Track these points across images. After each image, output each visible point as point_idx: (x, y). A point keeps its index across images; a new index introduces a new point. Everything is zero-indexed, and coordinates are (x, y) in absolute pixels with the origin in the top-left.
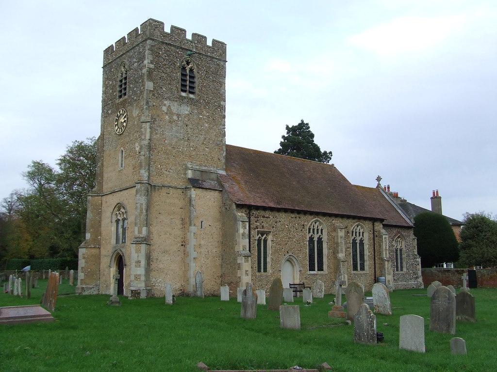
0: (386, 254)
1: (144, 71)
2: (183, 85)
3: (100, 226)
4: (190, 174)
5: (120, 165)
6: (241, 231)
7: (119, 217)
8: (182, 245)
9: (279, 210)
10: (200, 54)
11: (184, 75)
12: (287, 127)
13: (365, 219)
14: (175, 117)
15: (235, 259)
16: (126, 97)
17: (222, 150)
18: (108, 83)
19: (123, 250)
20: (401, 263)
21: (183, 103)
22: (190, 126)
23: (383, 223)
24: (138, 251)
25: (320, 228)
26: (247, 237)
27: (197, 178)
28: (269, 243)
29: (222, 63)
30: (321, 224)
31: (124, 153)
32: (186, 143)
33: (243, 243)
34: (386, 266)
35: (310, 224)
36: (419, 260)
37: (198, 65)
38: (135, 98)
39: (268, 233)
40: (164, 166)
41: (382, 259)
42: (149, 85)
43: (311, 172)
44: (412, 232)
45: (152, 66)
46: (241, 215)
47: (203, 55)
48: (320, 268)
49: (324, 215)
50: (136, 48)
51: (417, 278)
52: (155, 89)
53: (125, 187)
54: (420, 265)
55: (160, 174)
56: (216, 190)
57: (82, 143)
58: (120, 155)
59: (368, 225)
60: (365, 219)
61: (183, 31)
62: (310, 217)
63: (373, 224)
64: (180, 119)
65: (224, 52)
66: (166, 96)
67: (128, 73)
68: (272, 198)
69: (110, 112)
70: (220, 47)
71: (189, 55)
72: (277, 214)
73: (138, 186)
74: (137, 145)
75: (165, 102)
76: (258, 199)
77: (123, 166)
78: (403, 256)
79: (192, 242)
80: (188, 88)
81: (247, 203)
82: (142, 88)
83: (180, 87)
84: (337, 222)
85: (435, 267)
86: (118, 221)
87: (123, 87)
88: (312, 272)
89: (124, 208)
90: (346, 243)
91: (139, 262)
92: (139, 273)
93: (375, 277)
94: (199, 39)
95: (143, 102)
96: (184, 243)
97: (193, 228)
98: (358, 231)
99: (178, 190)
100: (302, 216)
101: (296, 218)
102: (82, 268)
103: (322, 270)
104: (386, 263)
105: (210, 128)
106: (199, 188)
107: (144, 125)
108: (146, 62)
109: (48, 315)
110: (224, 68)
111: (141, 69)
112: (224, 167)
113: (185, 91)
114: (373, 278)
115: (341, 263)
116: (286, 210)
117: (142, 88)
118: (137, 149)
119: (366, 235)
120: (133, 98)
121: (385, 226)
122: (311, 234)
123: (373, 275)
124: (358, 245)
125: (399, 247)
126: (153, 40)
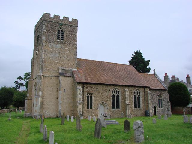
0: (150, 101)
4: (60, 71)
6: (78, 93)
10: (66, 24)
14: (55, 49)
15: (77, 104)
25: (118, 91)
28: (93, 98)
33: (79, 98)
34: (150, 106)
35: (113, 89)
36: (170, 103)
39: (92, 94)
41: (149, 104)
44: (167, 92)
46: (79, 87)
48: (118, 107)
60: (140, 87)
62: (113, 87)
70: (75, 21)
72: (97, 86)
75: (51, 44)
79: (60, 97)
83: (57, 38)
84: (126, 89)
92: (37, 109)
94: (66, 19)
97: (60, 92)
98: (137, 92)
103: (119, 108)
104: (150, 105)
110: (77, 29)
113: (59, 39)
114: (144, 111)
115: (127, 105)
121: (151, 90)
124: (137, 98)
125: (160, 98)
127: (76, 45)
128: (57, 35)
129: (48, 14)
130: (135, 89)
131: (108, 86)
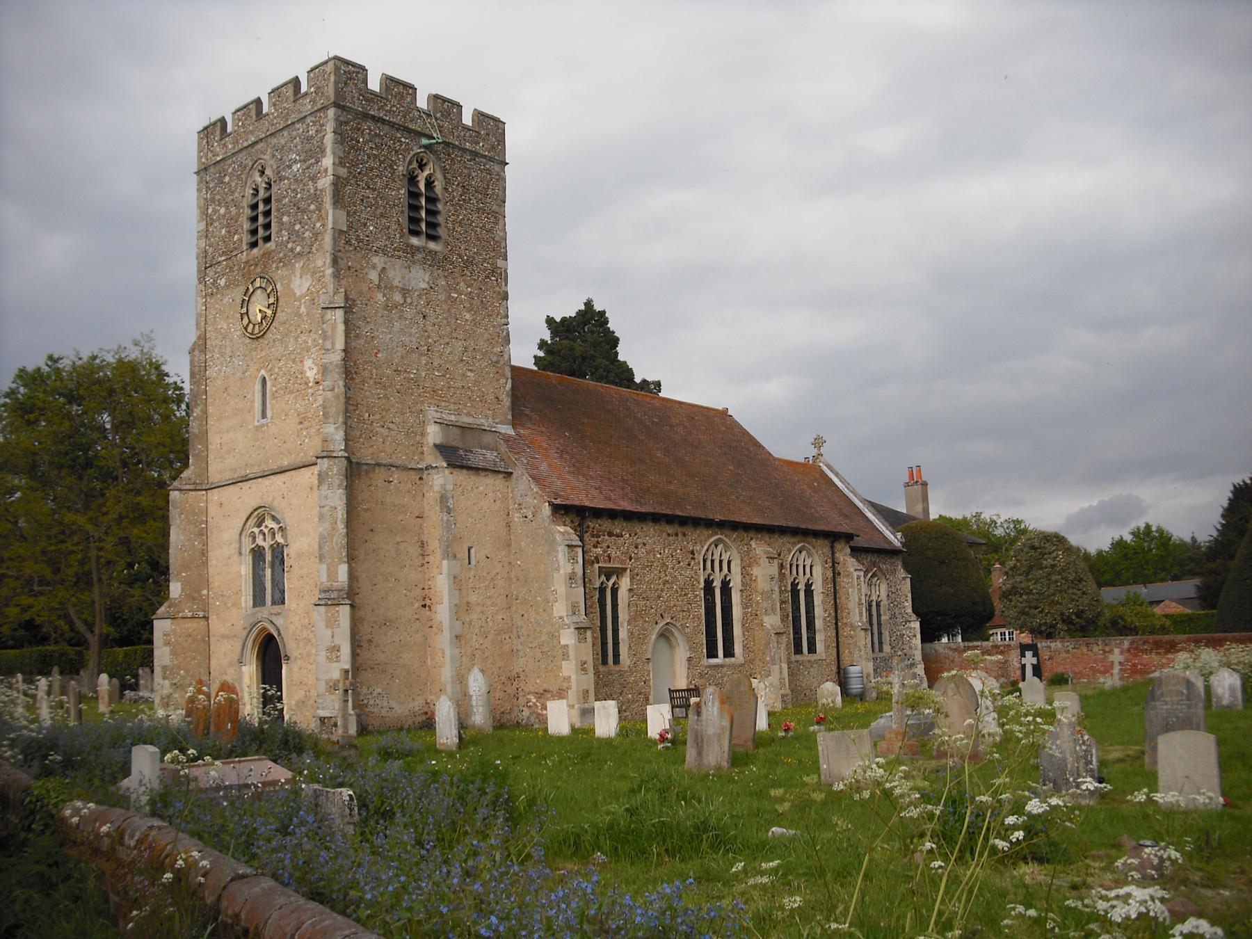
2: (414, 220)
3: (205, 564)
7: (260, 541)
8: (424, 606)
9: (641, 517)
11: (414, 195)
12: (550, 321)
13: (817, 534)
14: (398, 297)
16: (271, 245)
18: (215, 211)
19: (279, 621)
20: (880, 634)
21: (414, 263)
22: (432, 319)
23: (852, 543)
24: (331, 623)
27: (454, 444)
28: (623, 594)
29: (497, 168)
30: (727, 548)
31: (269, 384)
32: (424, 360)
37: (444, 170)
38: (298, 249)
39: (620, 572)
40: (378, 417)
43: (685, 427)
47: (454, 146)
49: (735, 526)
51: (912, 665)
52: (350, 227)
54: (919, 636)
56: (499, 472)
57: (94, 358)
58: (258, 387)
59: (822, 546)
60: (817, 534)
61: (410, 89)
62: (706, 532)
63: (832, 547)
64: (409, 301)
65: (501, 140)
67: (274, 188)
68: (623, 489)
69: (222, 282)
71: (425, 147)
72: (637, 528)
73: (324, 464)
74: (308, 363)
76: (595, 493)
78: (883, 618)
80: (423, 226)
81: (577, 503)
82: (318, 225)
84: (760, 547)
85: (945, 640)
86: (258, 554)
87: (261, 220)
88: (713, 661)
89: (274, 518)
90: (781, 592)
91: (336, 649)
93: (839, 667)
94: (446, 107)
99: (411, 473)
100: (689, 530)
101: (677, 535)
103: (733, 655)
105: (475, 323)
106: (462, 467)
107: (329, 314)
110: (501, 179)
111: (314, 179)
112: (510, 417)
116: (656, 518)
117: (318, 225)
119: (818, 571)
120: (292, 250)
121: (856, 551)
122: (75, 548)
123: (835, 663)
125: (874, 598)
127: (502, 276)
128: (406, 209)
129: (354, 65)
130: (794, 544)
131: (684, 530)
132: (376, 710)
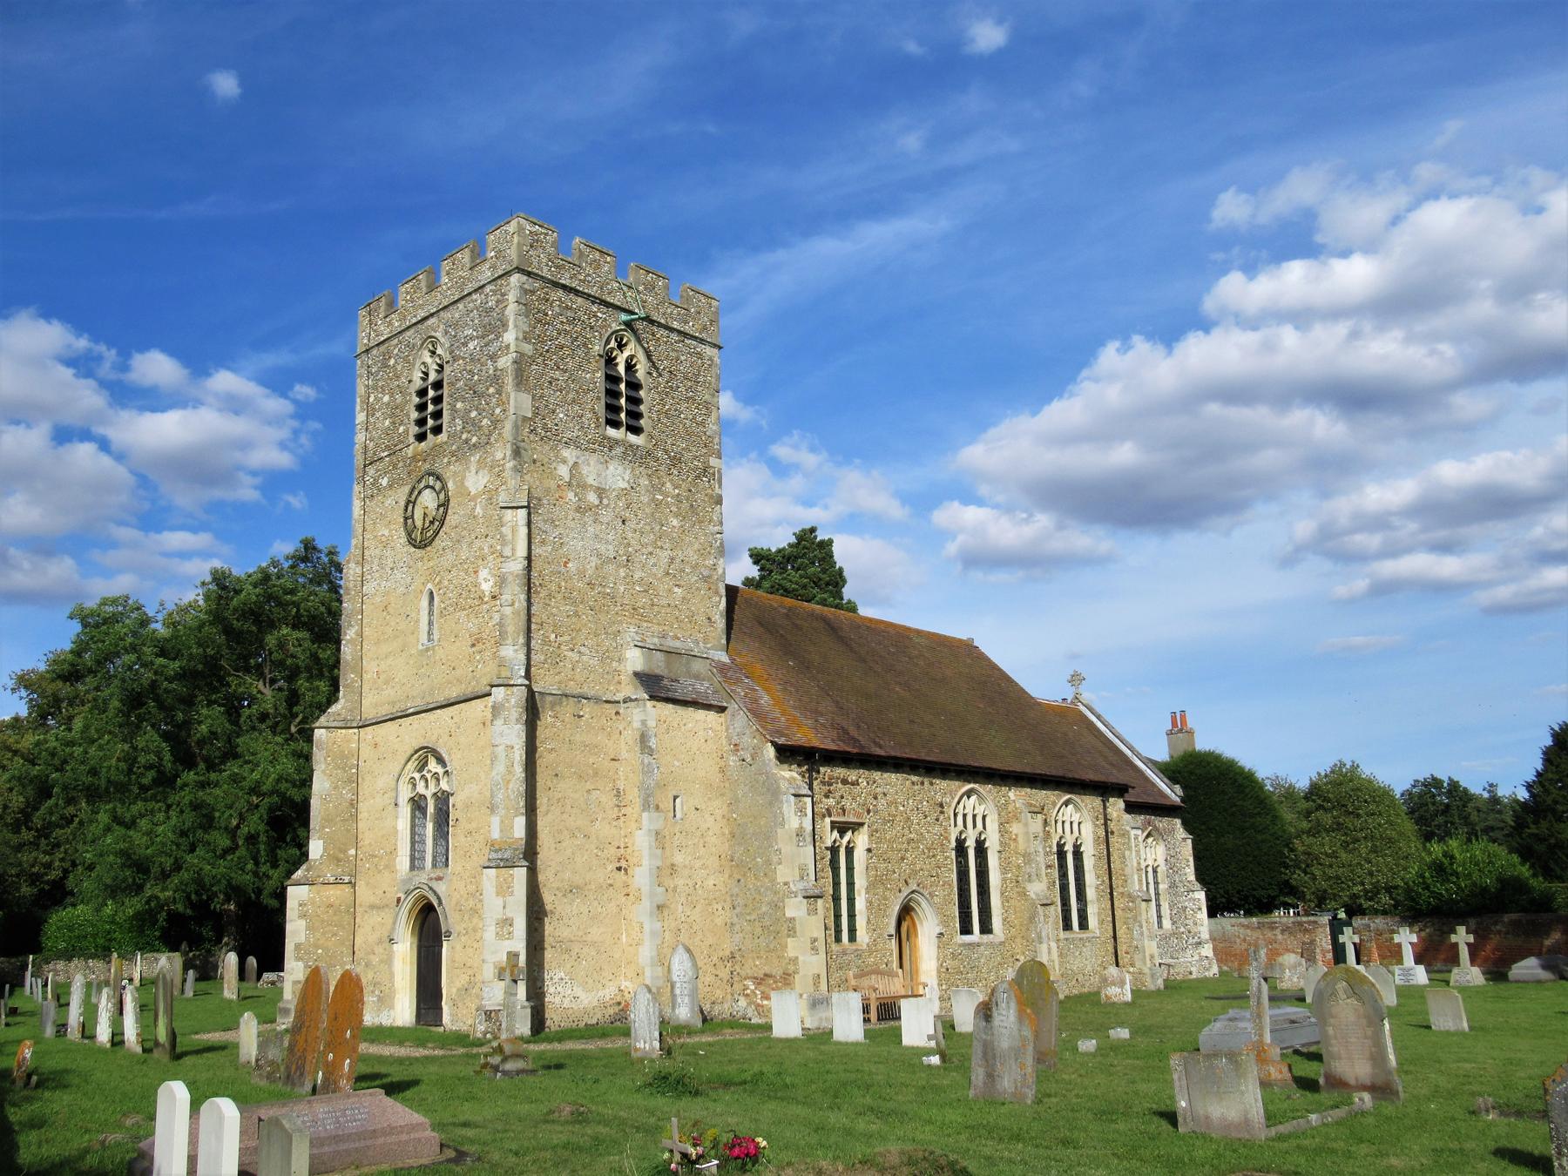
1: (505, 362)
2: (612, 409)
5: (424, 637)
6: (793, 822)
7: (421, 789)
8: (619, 869)
11: (612, 379)
14: (592, 498)
16: (443, 437)
17: (717, 593)
19: (441, 888)
23: (1128, 797)
26: (809, 839)
28: (860, 856)
38: (474, 439)
39: (855, 827)
40: (566, 638)
42: (519, 402)
45: (528, 349)
46: (790, 775)
50: (474, 297)
53: (441, 699)
55: (556, 660)
58: (425, 603)
59: (1092, 802)
64: (605, 501)
66: (568, 435)
67: (447, 369)
69: (384, 482)
73: (499, 693)
74: (484, 573)
77: (436, 637)
82: (498, 411)
87: (431, 408)
88: (967, 938)
89: (441, 761)
91: (508, 922)
95: (501, 452)
96: (623, 864)
98: (969, 811)
102: (298, 947)
108: (510, 337)
109: (414, 1127)
111: (493, 357)
117: (498, 411)
118: (487, 587)
126: (529, 274)
132: (557, 1000)
